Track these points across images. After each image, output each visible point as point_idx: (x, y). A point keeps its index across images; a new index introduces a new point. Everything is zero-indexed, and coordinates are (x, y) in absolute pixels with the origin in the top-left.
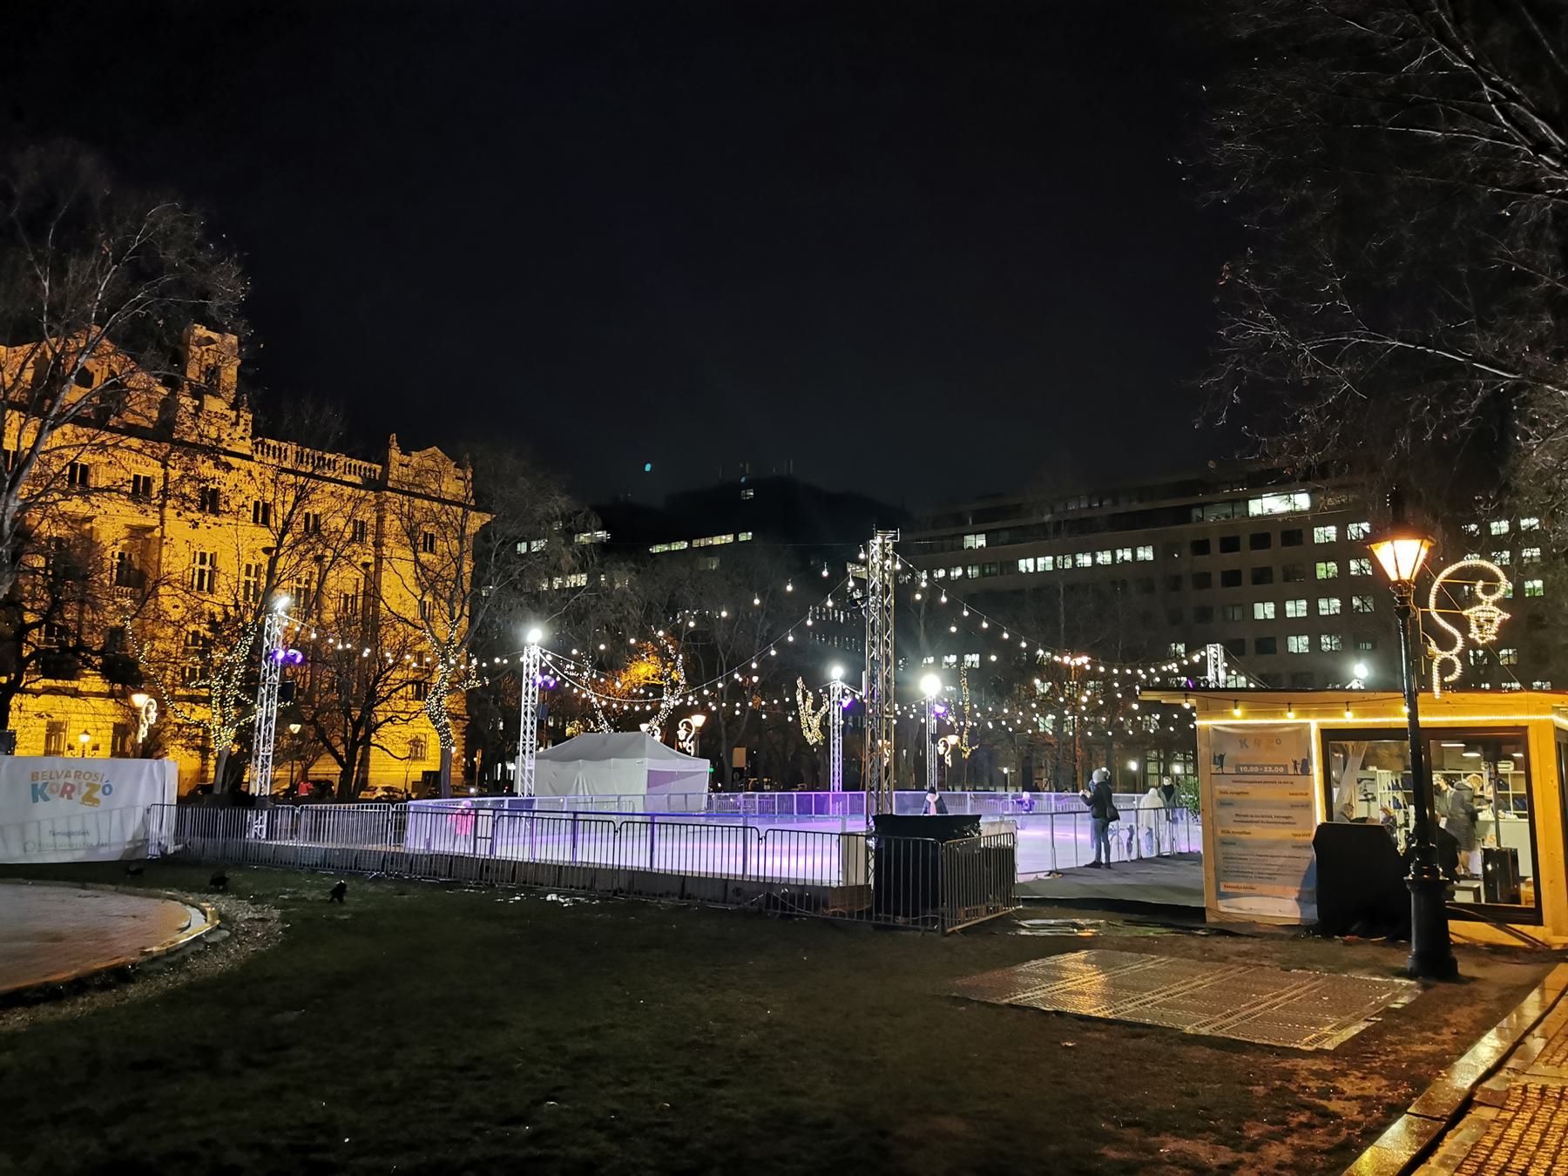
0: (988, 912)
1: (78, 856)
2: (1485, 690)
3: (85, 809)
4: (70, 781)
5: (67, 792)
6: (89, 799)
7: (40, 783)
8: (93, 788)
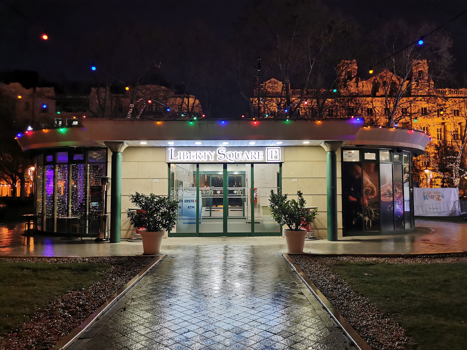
0: (90, 175)
1: (436, 215)
2: (434, 228)
3: (437, 202)
4: (433, 194)
5: (432, 197)
6: (438, 199)
7: (425, 195)
8: (439, 196)
